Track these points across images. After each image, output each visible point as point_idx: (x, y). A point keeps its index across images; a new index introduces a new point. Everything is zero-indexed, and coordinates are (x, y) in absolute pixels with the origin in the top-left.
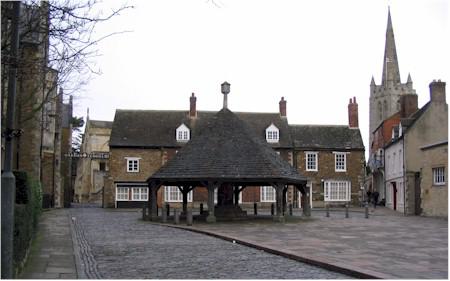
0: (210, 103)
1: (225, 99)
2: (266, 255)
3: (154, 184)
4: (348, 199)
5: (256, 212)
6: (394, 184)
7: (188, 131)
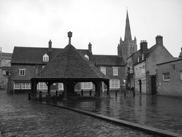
0: (60, 43)
1: (70, 40)
2: (112, 127)
3: (34, 82)
4: (119, 87)
6: (140, 81)
7: (48, 57)
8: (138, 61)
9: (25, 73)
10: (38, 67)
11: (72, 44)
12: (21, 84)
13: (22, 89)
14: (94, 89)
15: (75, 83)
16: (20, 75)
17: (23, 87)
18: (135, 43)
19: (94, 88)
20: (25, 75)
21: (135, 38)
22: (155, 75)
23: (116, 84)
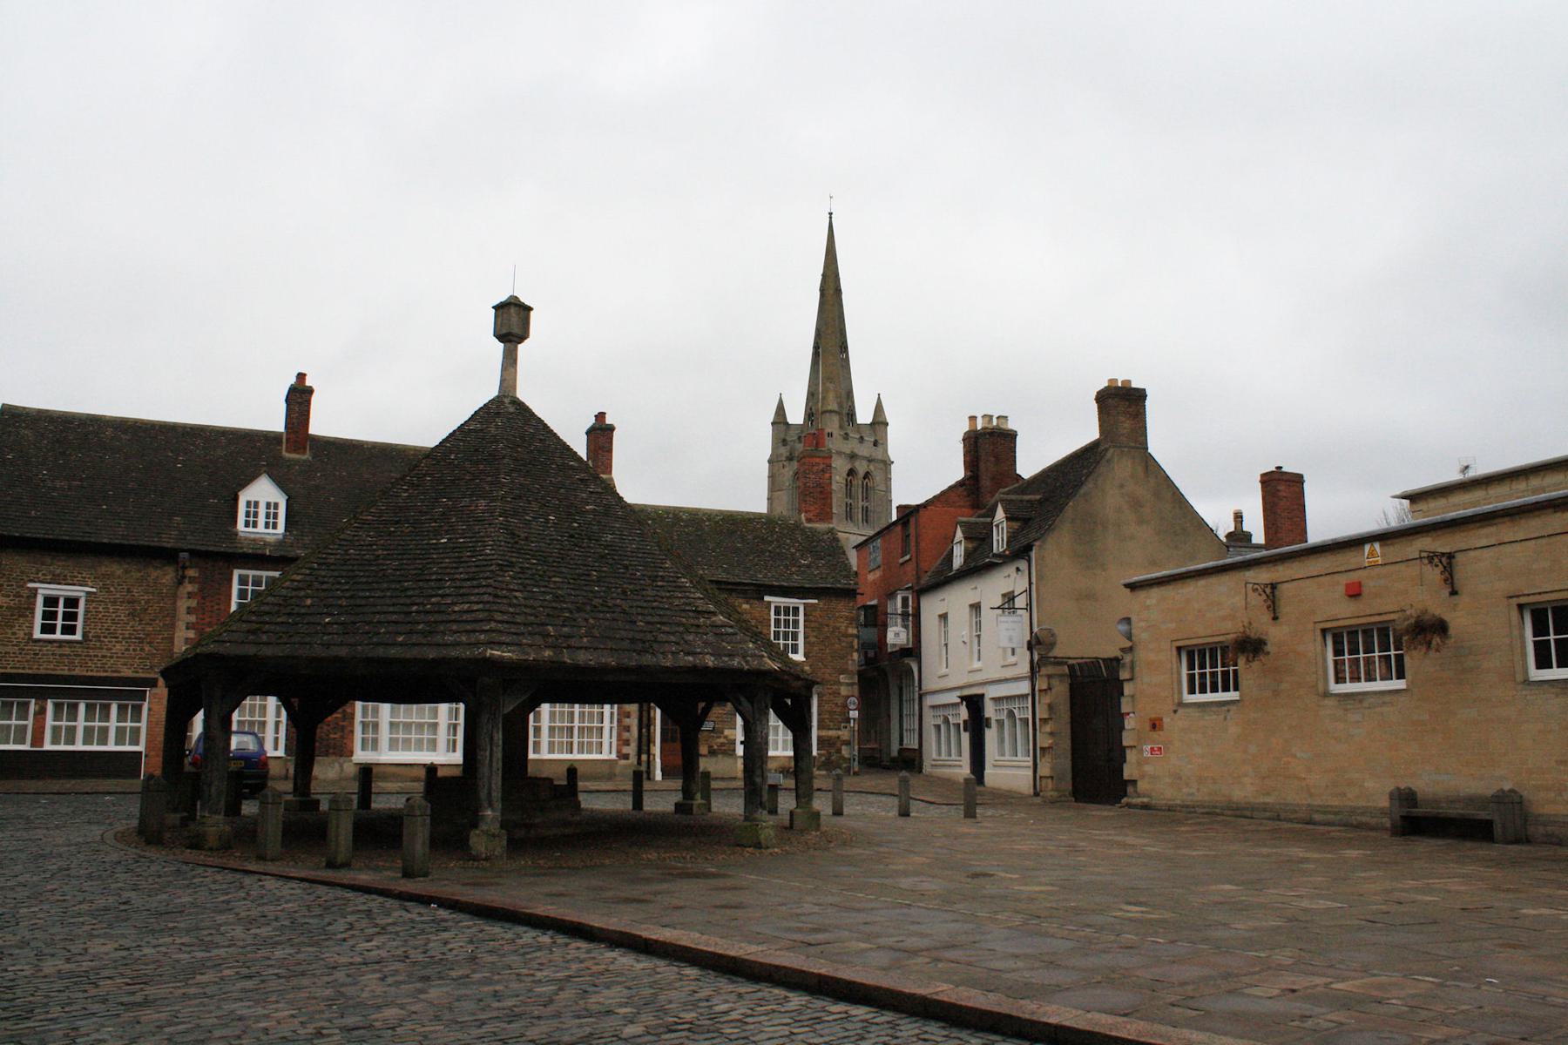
1: (510, 361)
5: (638, 803)
6: (974, 703)
8: (958, 561)
9: (80, 624)
10: (192, 573)
11: (522, 394)
12: (41, 712)
13: (48, 746)
14: (626, 757)
15: (702, 705)
16: (37, 634)
17: (56, 730)
18: (875, 444)
19: (625, 750)
20: (78, 637)
21: (879, 408)
22: (1114, 663)
23: (590, 729)
